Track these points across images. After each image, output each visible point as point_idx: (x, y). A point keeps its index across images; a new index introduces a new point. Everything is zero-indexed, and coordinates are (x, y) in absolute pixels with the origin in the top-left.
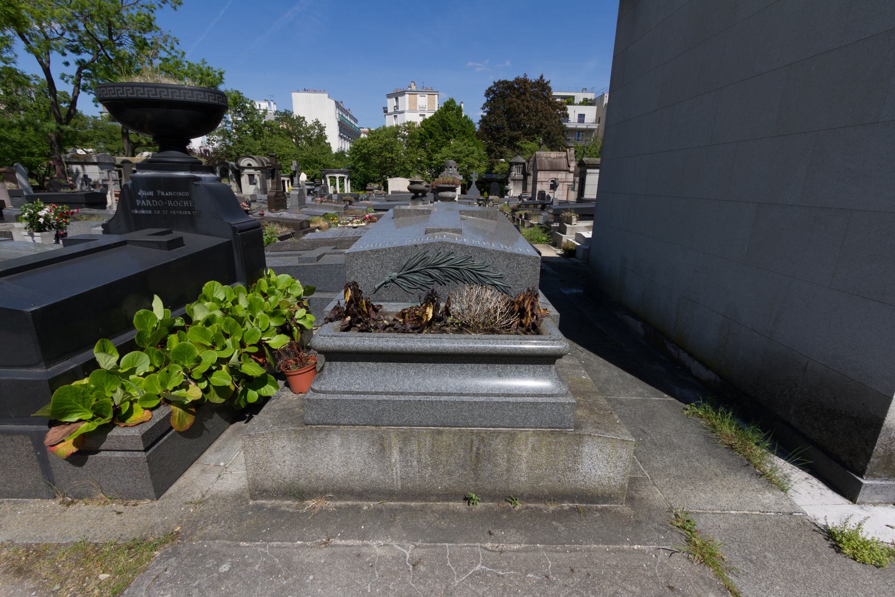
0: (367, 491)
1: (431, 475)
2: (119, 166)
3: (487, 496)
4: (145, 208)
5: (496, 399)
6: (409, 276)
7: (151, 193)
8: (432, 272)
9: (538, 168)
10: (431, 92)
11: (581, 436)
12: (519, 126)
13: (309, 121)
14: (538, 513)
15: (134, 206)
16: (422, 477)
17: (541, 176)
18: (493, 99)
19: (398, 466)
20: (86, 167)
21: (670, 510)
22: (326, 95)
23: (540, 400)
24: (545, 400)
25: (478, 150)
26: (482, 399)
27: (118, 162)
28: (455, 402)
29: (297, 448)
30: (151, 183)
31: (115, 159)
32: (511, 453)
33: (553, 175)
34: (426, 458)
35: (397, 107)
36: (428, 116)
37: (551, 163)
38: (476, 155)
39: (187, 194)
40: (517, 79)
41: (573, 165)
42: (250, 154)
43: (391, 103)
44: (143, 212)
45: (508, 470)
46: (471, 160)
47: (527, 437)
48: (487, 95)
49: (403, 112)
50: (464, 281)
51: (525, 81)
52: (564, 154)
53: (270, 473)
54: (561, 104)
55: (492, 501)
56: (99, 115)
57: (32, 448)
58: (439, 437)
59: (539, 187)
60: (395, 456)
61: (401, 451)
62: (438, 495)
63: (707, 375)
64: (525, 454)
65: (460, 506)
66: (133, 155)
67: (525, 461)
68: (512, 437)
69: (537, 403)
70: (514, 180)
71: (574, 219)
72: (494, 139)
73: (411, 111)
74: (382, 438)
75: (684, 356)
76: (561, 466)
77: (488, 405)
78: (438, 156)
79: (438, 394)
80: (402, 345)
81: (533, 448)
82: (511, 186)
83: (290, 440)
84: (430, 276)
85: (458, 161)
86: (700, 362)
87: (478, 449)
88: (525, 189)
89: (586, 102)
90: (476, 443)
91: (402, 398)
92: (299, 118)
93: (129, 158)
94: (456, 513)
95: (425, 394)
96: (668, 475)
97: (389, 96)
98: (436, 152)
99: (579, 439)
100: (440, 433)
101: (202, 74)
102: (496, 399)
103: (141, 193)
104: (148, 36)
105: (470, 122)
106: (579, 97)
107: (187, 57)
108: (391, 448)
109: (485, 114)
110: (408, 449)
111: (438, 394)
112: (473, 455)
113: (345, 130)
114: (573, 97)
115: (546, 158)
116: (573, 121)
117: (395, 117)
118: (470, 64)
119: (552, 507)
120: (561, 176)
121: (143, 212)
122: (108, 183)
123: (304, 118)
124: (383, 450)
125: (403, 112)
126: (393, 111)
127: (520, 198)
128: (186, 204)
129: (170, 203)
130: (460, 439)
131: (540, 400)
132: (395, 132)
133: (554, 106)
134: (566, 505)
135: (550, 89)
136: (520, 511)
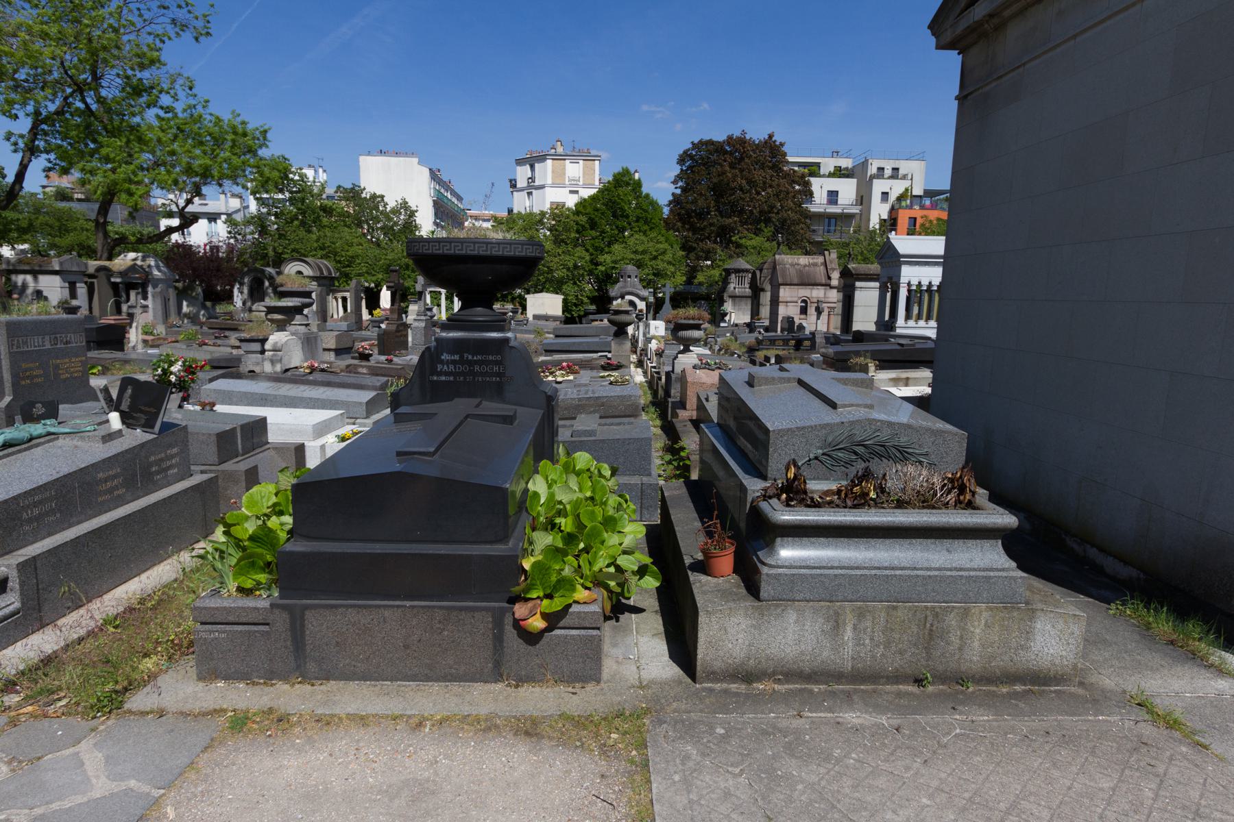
0: (815, 673)
1: (883, 655)
2: (91, 276)
3: (941, 678)
4: (447, 374)
5: (949, 573)
6: (834, 454)
7: (457, 357)
8: (858, 449)
9: (780, 281)
10: (588, 157)
11: (1034, 611)
12: (736, 210)
13: (391, 202)
14: (993, 695)
15: (434, 372)
16: (873, 657)
17: (784, 293)
18: (690, 167)
19: (850, 646)
20: (41, 278)
21: (1124, 692)
22: (415, 160)
23: (992, 574)
24: (997, 574)
25: (668, 248)
26: (936, 573)
27: (91, 270)
28: (909, 576)
29: (753, 626)
30: (458, 346)
31: (86, 265)
32: (964, 629)
33: (804, 292)
34: (879, 636)
35: (532, 179)
36: (586, 193)
37: (800, 273)
38: (668, 257)
39: (499, 358)
40: (730, 138)
41: (835, 276)
42: (300, 257)
43: (522, 174)
44: (443, 378)
45: (960, 649)
46: (661, 265)
47: (981, 612)
48: (681, 161)
49: (542, 187)
50: (889, 458)
51: (742, 141)
52: (820, 259)
53: (721, 653)
54: (803, 176)
55: (943, 684)
56: (40, 190)
57: (490, 626)
58: (894, 613)
59: (783, 311)
60: (849, 633)
61: (855, 628)
62: (888, 677)
63: (1125, 572)
64: (978, 631)
65: (912, 688)
66: (110, 258)
67: (977, 639)
68: (966, 613)
69: (990, 577)
70: (733, 297)
71: (872, 367)
72: (694, 230)
73: (554, 185)
74: (837, 614)
75: (1093, 553)
76: (1014, 645)
77: (942, 579)
78: (607, 258)
79: (893, 569)
80: (860, 519)
81: (986, 625)
82: (728, 306)
83: (746, 615)
84: (855, 453)
85: (639, 265)
86: (1115, 557)
87: (932, 625)
88: (755, 313)
89: (839, 173)
90: (930, 618)
91: (859, 572)
92: (374, 196)
93: (107, 263)
94: (908, 694)
95: (879, 568)
96: (1112, 666)
97: (520, 162)
98: (602, 251)
99: (1032, 614)
100: (895, 608)
101: (235, 133)
102: (949, 573)
103: (445, 357)
104: (146, 75)
105: (654, 204)
106: (828, 165)
107: (212, 108)
108: (845, 624)
109: (678, 191)
110: (862, 626)
111: (893, 569)
112: (927, 632)
113: (442, 210)
114: (818, 165)
115: (792, 265)
116: (819, 202)
117: (530, 194)
118: (645, 108)
119: (1005, 690)
120: (817, 293)
121: (443, 378)
122: (134, 311)
123: (382, 197)
124: (837, 626)
125: (542, 187)
126: (525, 185)
127: (751, 327)
128: (496, 369)
129: (477, 368)
130: (914, 615)
131: (992, 574)
132: (533, 221)
133: (792, 178)
134: (1018, 688)
135: (785, 154)
136: (973, 693)
